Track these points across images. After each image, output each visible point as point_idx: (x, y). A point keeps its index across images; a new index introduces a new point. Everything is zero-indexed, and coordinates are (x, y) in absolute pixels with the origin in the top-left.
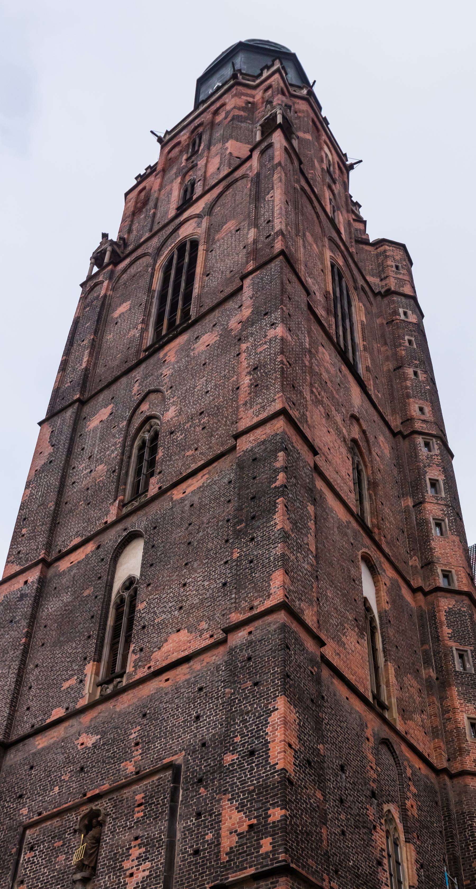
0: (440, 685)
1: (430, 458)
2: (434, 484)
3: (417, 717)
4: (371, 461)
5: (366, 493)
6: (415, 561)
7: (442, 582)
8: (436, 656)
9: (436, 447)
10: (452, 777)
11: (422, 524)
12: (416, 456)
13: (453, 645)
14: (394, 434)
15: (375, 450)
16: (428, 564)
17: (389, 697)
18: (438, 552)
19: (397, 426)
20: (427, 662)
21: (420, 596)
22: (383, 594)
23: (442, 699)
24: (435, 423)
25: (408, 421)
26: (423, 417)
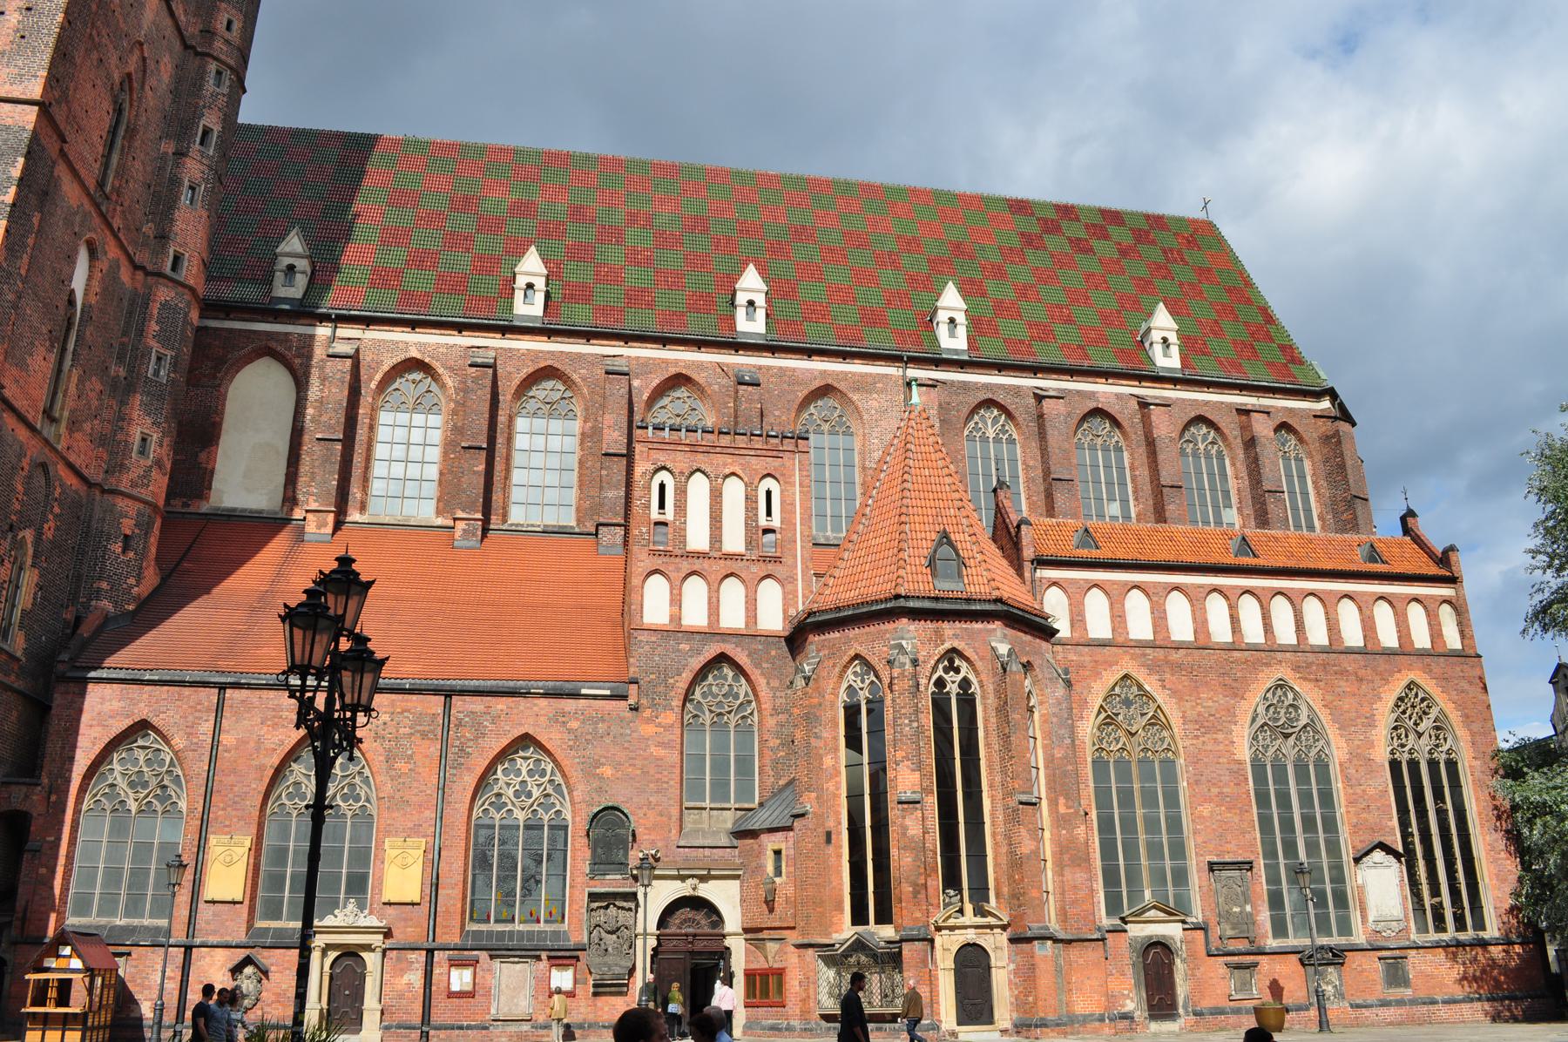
0: (122, 390)
1: (214, 95)
2: (207, 132)
3: (87, 426)
4: (140, 99)
5: (119, 142)
6: (149, 229)
7: (167, 269)
8: (132, 355)
9: (227, 83)
10: (103, 491)
11: (175, 182)
12: (201, 88)
13: (155, 346)
14: (186, 46)
15: (151, 81)
16: (163, 237)
17: (62, 409)
18: (179, 225)
19: (193, 36)
20: (120, 358)
21: (140, 275)
22: (95, 283)
23: (123, 403)
24: (239, 49)
25: (208, 33)
26: (227, 35)
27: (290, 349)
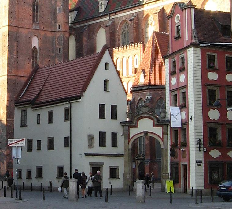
27: (103, 25)
